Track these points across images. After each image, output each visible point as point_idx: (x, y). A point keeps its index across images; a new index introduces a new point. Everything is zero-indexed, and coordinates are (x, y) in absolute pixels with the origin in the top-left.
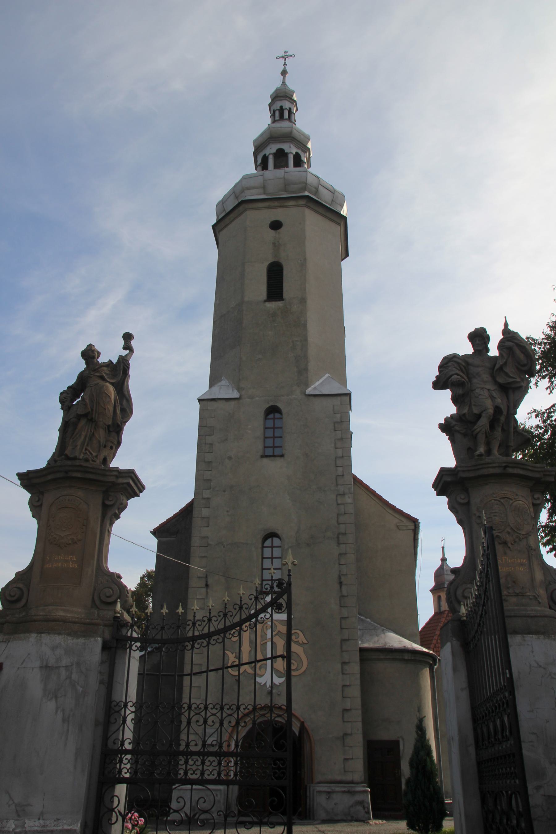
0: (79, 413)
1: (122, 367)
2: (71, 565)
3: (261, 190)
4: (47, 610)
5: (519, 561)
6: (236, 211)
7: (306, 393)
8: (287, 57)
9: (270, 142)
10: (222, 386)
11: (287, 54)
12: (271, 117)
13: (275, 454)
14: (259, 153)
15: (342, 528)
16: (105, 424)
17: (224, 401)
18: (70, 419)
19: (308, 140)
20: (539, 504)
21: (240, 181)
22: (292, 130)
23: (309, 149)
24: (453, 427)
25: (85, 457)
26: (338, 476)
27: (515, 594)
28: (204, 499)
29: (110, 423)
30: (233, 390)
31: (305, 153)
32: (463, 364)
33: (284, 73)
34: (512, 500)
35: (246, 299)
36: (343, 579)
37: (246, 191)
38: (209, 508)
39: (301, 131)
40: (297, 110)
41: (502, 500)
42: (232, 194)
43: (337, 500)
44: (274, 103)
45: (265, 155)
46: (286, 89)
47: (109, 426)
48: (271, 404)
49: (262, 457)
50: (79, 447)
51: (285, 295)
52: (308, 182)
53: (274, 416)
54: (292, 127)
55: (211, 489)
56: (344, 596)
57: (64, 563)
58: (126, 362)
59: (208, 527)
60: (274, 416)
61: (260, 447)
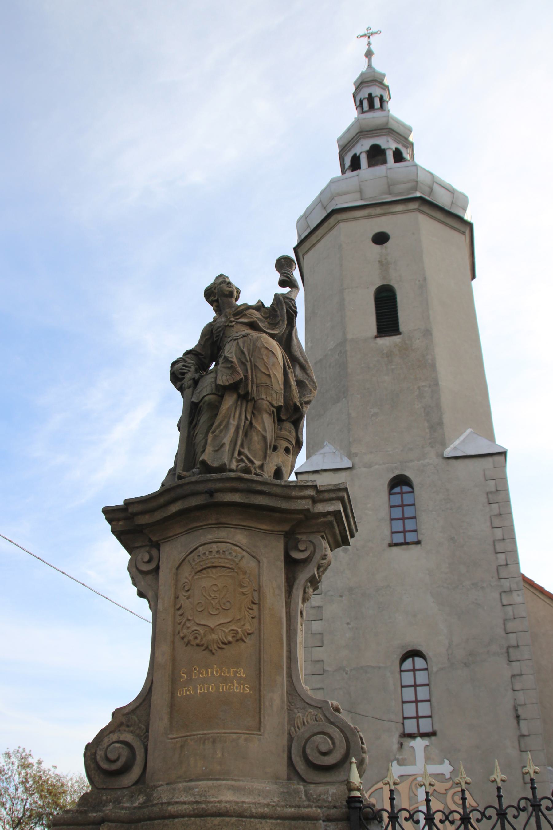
0: (220, 382)
1: (285, 310)
2: (237, 689)
3: (358, 195)
4: (196, 790)
7: (444, 456)
10: (326, 454)
11: (371, 31)
12: (358, 109)
13: (407, 541)
14: (346, 154)
15: (513, 639)
16: (272, 406)
18: (204, 396)
22: (388, 120)
25: (239, 467)
26: (501, 566)
28: (314, 607)
29: (281, 403)
30: (341, 459)
33: (369, 54)
35: (349, 336)
36: (520, 712)
38: (321, 620)
43: (501, 599)
45: (355, 155)
47: (279, 409)
48: (397, 473)
49: (390, 545)
50: (227, 447)
51: (402, 328)
52: (419, 179)
53: (401, 489)
54: (388, 116)
55: (323, 595)
56: (524, 736)
57: (221, 685)
58: (291, 302)
59: (322, 646)
60: (401, 489)
61: (387, 532)
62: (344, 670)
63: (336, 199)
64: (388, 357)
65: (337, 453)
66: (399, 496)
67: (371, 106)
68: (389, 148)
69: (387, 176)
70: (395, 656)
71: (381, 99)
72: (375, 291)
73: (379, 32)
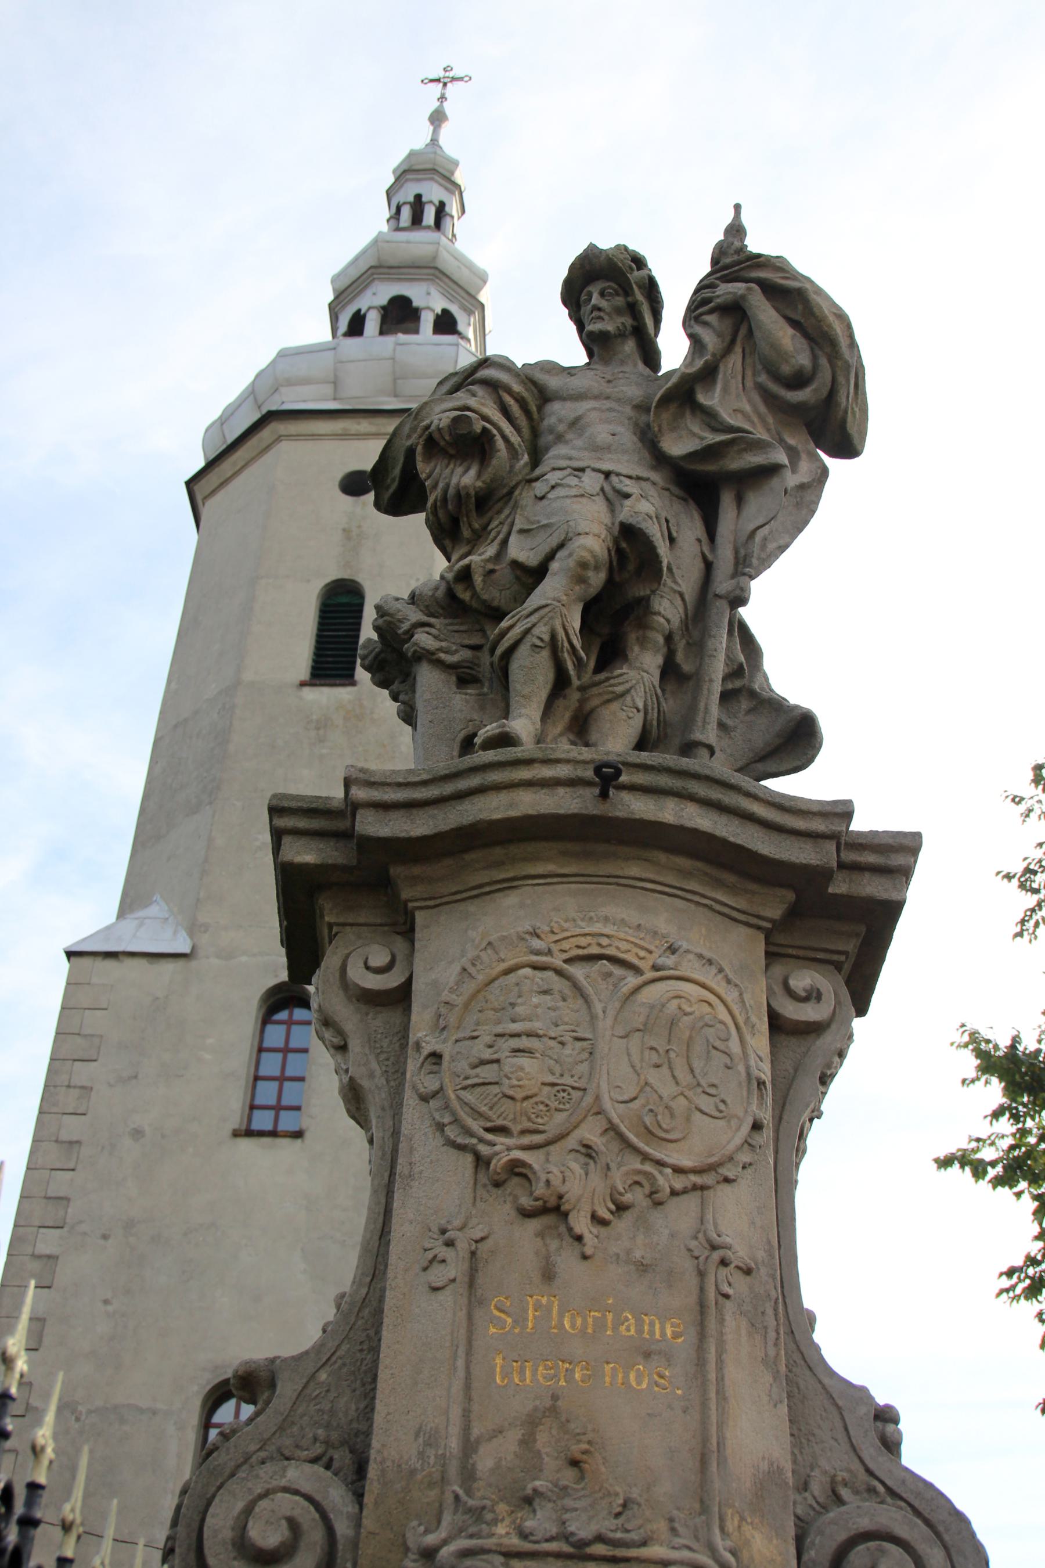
3: (328, 389)
5: (629, 1329)
6: (253, 442)
8: (451, 81)
9: (375, 276)
11: (451, 74)
14: (344, 307)
17: (143, 962)
19: (480, 282)
20: (813, 1029)
21: (273, 363)
22: (437, 251)
23: (483, 306)
24: (410, 634)
27: (566, 1548)
28: (39, 1257)
30: (175, 933)
31: (469, 316)
32: (517, 388)
33: (437, 118)
34: (637, 970)
35: (248, 676)
37: (283, 390)
38: (49, 1287)
39: (463, 256)
40: (463, 212)
41: (578, 971)
42: (248, 397)
44: (401, 187)
46: (435, 153)
53: (291, 1015)
54: (439, 243)
55: (65, 1229)
59: (36, 1350)
62: (74, 1411)
63: (283, 390)
64: (318, 729)
65: (170, 920)
66: (284, 1027)
67: (417, 220)
68: (428, 308)
69: (393, 359)
70: (196, 1388)
71: (441, 210)
72: (322, 590)
73: (466, 79)
